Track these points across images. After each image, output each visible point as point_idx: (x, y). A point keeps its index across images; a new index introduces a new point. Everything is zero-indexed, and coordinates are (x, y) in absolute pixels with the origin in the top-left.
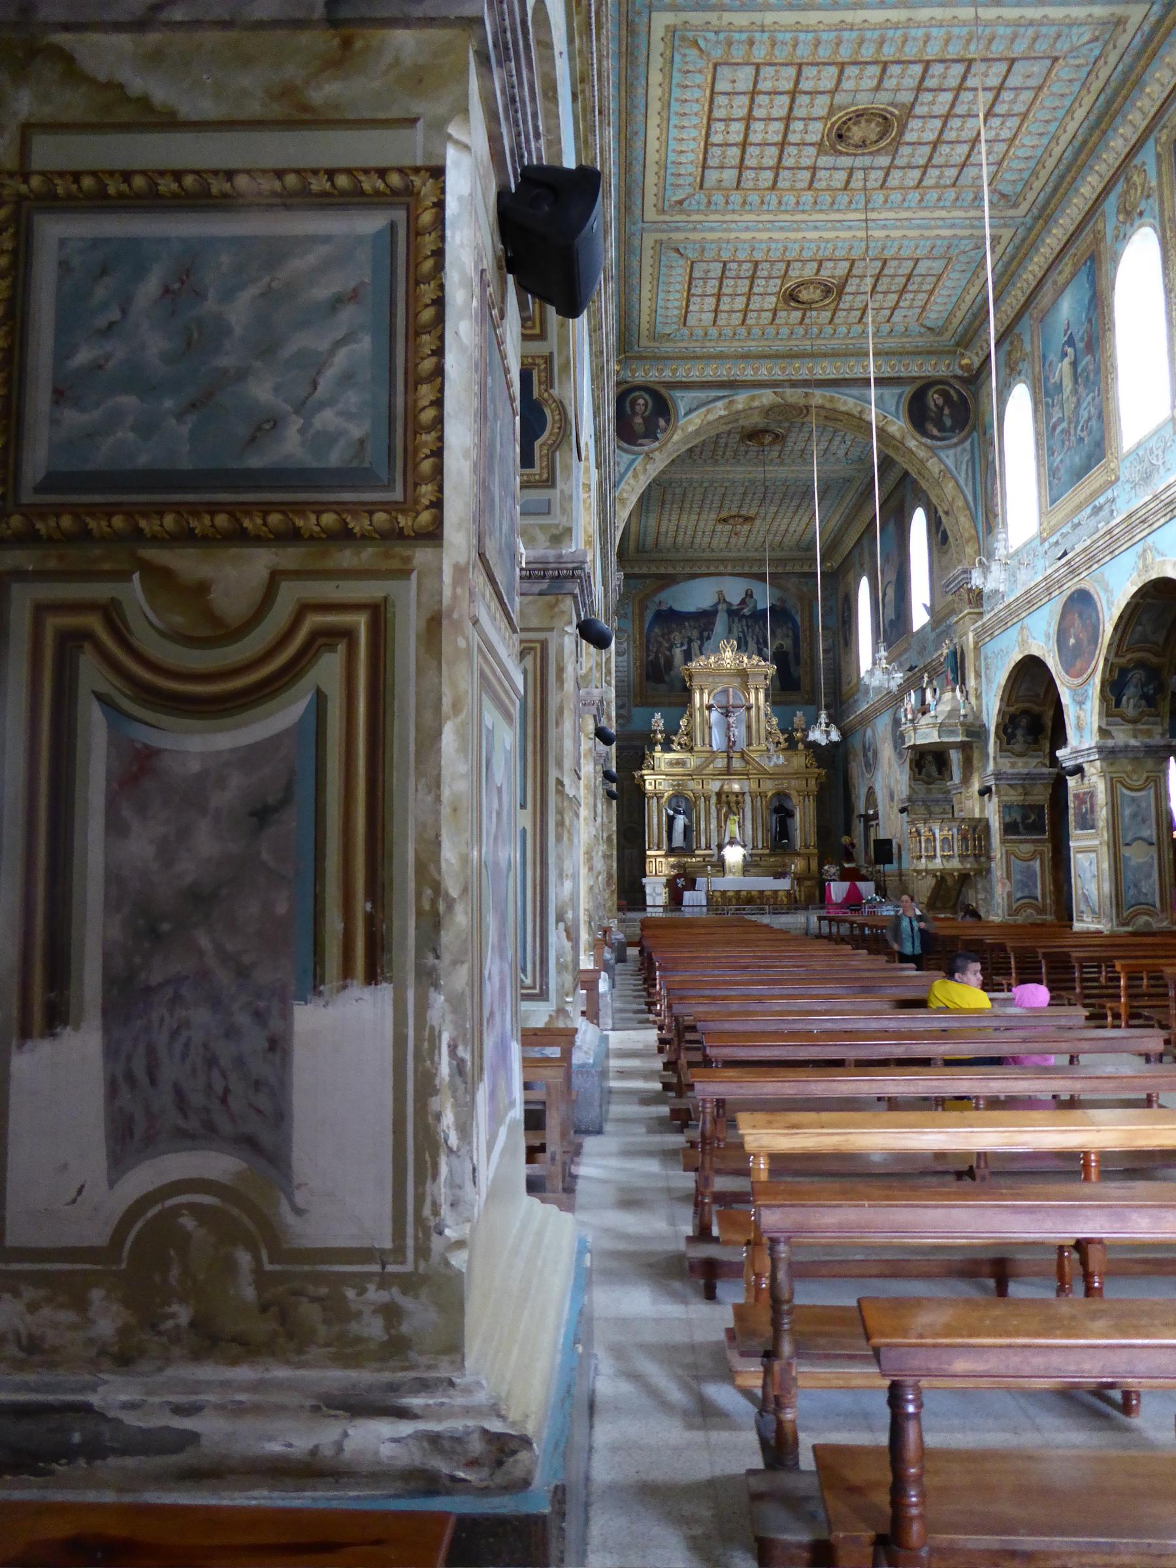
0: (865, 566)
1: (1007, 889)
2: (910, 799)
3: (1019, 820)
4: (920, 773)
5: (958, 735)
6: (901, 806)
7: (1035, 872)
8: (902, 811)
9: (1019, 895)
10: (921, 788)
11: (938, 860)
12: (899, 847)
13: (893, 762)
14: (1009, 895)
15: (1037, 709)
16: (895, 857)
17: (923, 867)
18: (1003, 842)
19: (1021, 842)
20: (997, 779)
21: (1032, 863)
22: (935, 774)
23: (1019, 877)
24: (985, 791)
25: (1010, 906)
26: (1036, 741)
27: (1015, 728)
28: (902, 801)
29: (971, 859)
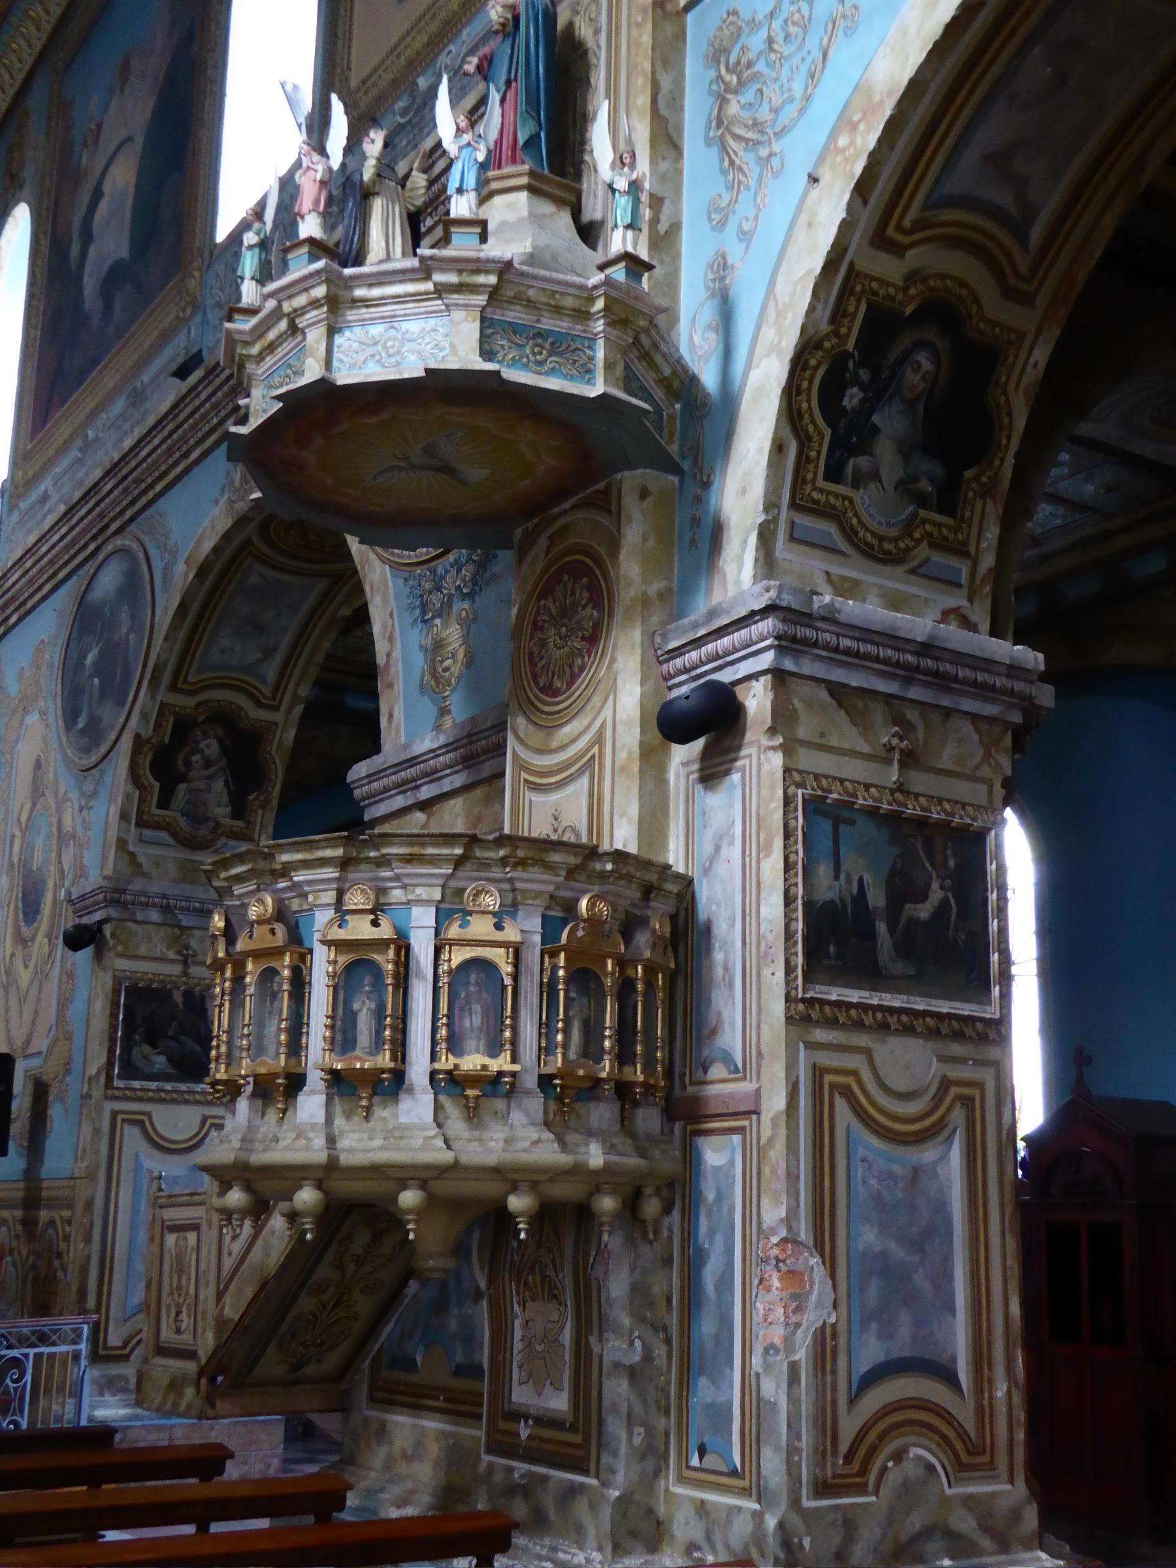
0: (29, 173)
1: (811, 1319)
2: (115, 895)
3: (877, 898)
4: (164, 802)
5: (586, 372)
6: (69, 921)
7: (941, 1208)
8: (77, 939)
9: (872, 1351)
10: (162, 858)
11: (417, 1107)
12: (40, 1091)
13: (60, 777)
14: (825, 1347)
15: (994, 308)
16: (18, 1127)
17: (315, 1151)
18: (804, 1015)
19: (886, 1023)
20: (786, 644)
21: (928, 1154)
22: (221, 812)
23: (869, 1237)
24: (705, 722)
25: (826, 1425)
26: (948, 500)
27: (876, 396)
28: (80, 904)
29: (602, 1113)
